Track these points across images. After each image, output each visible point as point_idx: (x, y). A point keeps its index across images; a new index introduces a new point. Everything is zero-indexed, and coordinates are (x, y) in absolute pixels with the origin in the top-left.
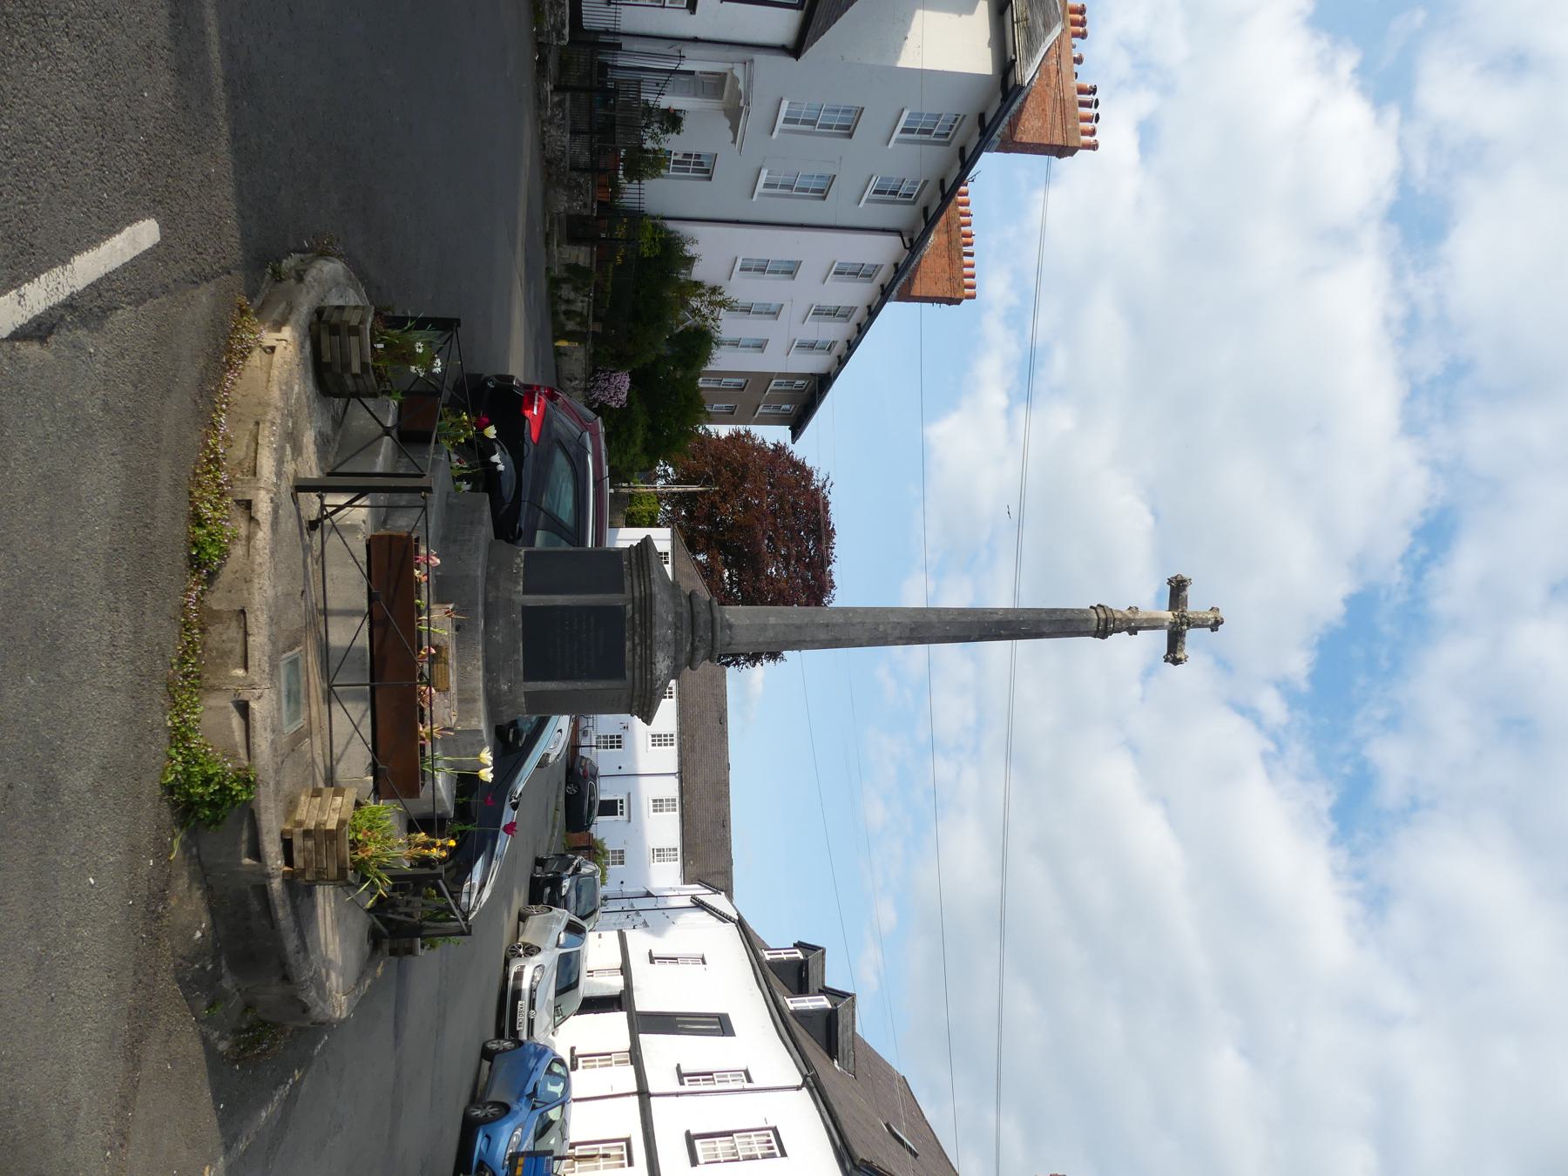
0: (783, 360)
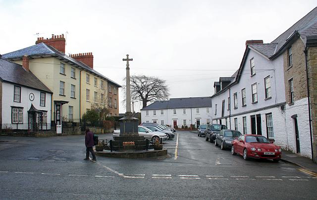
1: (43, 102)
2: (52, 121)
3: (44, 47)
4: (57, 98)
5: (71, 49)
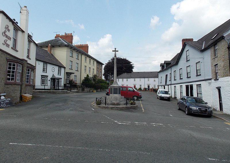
0: (95, 66)
1: (59, 72)
2: (64, 84)
3: (60, 40)
4: (68, 70)
5: (76, 41)
